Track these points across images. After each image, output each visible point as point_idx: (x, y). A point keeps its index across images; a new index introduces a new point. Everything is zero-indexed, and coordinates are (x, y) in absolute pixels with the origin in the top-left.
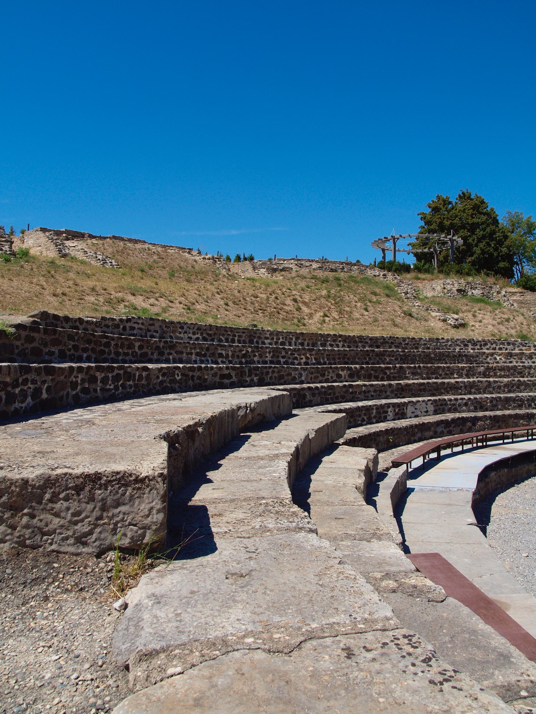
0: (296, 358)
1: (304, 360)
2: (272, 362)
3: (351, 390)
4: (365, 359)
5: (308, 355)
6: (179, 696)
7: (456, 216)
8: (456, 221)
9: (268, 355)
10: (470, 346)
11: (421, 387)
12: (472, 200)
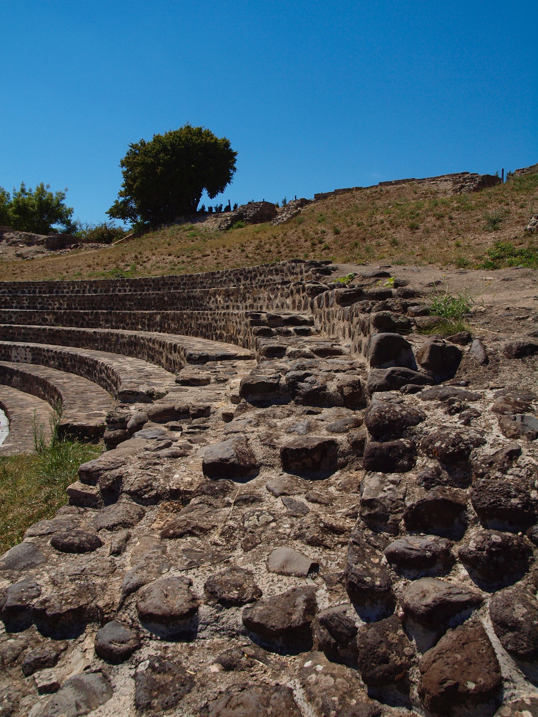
0: (50, 304)
1: (57, 306)
2: (28, 308)
3: (11, 331)
4: (110, 304)
5: (61, 301)
9: (25, 302)
11: (69, 335)
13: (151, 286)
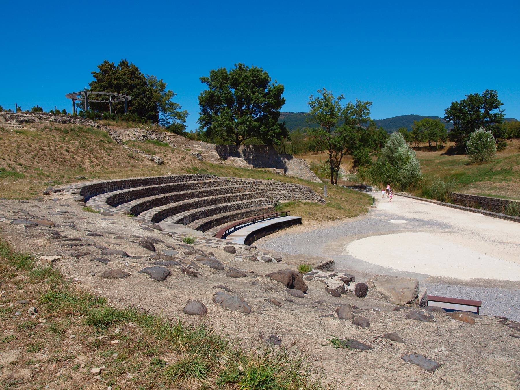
6: (428, 187)
7: (120, 78)
8: (120, 81)
10: (185, 180)
12: (129, 67)
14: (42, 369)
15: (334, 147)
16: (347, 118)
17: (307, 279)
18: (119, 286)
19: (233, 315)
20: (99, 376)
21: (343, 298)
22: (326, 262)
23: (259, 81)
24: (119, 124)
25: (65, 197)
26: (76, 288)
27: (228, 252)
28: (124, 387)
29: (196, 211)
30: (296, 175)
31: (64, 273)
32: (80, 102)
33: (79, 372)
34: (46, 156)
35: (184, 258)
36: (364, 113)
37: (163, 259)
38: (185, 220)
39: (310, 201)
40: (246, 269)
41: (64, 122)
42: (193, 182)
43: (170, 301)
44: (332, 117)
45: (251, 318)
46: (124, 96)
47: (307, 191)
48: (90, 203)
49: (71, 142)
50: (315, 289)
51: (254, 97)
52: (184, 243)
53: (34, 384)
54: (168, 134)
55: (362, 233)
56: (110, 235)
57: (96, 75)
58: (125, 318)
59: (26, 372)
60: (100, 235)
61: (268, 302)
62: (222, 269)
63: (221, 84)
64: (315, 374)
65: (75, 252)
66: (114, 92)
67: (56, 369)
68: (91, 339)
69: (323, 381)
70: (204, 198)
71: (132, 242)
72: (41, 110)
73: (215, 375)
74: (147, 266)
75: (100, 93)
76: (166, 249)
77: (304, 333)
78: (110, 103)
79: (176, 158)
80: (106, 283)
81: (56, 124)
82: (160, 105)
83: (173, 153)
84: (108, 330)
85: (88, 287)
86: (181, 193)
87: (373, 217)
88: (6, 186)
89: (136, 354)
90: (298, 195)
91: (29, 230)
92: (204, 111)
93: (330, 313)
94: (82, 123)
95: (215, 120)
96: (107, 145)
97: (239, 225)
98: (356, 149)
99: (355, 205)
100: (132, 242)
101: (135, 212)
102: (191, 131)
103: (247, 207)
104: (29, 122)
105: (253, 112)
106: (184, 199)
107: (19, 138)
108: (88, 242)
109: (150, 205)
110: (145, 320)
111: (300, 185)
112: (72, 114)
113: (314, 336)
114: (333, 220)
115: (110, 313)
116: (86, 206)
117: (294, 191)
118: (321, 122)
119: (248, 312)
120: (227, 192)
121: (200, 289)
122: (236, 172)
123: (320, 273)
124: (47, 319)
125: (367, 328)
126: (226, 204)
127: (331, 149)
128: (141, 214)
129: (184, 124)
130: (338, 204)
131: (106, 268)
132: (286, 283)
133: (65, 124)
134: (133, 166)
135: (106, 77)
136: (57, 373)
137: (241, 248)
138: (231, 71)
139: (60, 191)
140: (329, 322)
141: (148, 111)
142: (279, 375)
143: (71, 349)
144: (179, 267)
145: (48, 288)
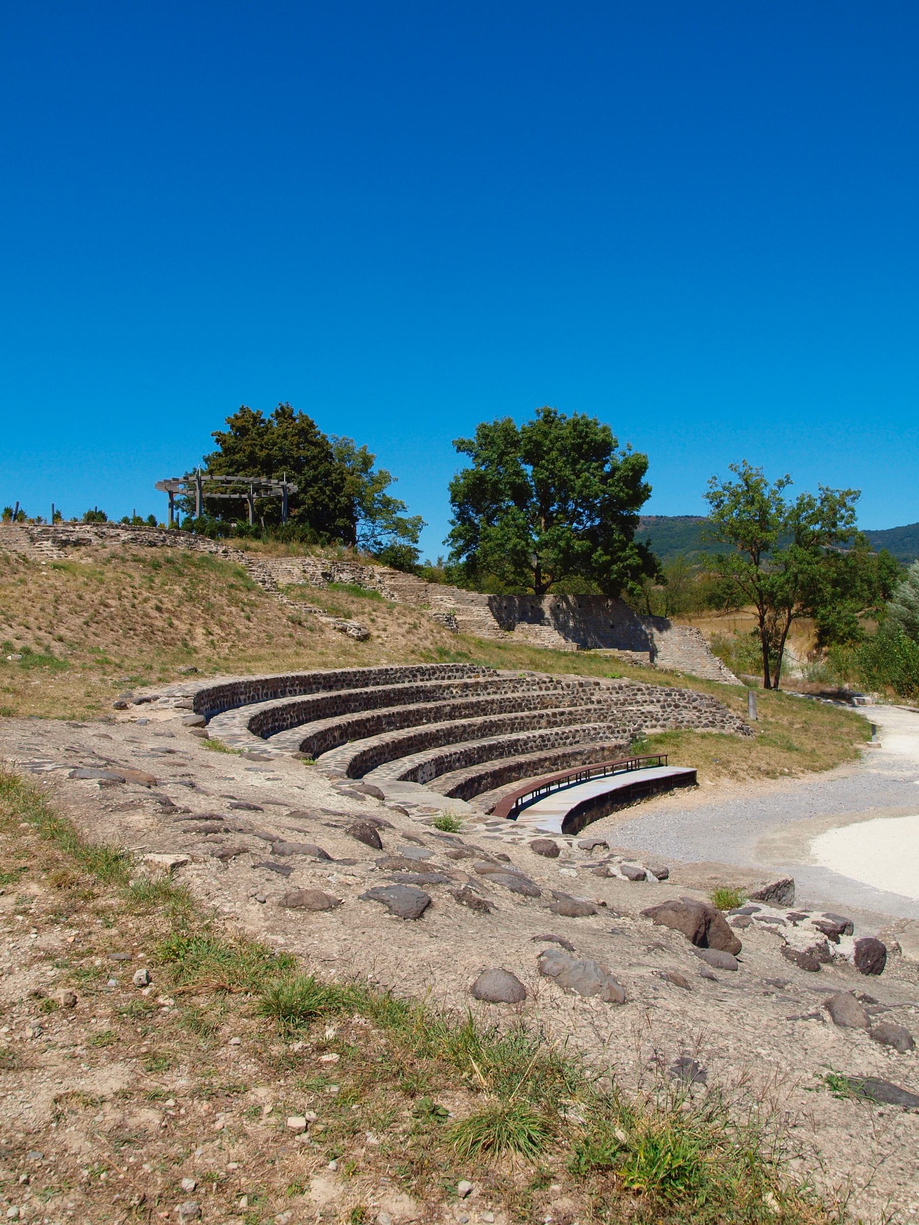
7: (275, 444)
8: (275, 452)
12: (295, 419)
13: (320, 683)
14: (183, 1111)
15: (767, 599)
16: (799, 530)
17: (737, 923)
18: (320, 929)
19: (586, 1006)
20: (305, 1136)
21: (827, 974)
22: (773, 883)
23: (591, 447)
24: (269, 547)
25: (162, 716)
26: (226, 929)
27: (540, 853)
28: (362, 1164)
29: (446, 750)
30: (678, 667)
31: (198, 894)
32: (183, 497)
33: (262, 1123)
34: (112, 619)
35: (448, 866)
36: (842, 517)
37: (410, 869)
38: (420, 773)
39: (715, 731)
40: (587, 895)
41: (152, 544)
42: (439, 682)
43: (439, 967)
44: (762, 529)
45: (628, 1014)
46: (281, 485)
47: (708, 706)
48: (214, 729)
49: (167, 588)
50: (758, 949)
51: (579, 482)
52: (438, 831)
53: (171, 1145)
54: (379, 569)
55: (849, 811)
56: (277, 807)
57: (220, 439)
58: (344, 1004)
59: (149, 1117)
60: (256, 809)
61: (662, 977)
62: (538, 894)
63: (502, 454)
64: (800, 1161)
65: (217, 847)
66: (259, 475)
67: (211, 1114)
68: (277, 1049)
69: (818, 1178)
70: (464, 721)
71: (327, 825)
72: (103, 517)
73: (562, 1148)
74: (377, 885)
75: (229, 478)
76: (403, 842)
77: (758, 1056)
78: (251, 499)
79: (399, 625)
80: (291, 921)
81: (135, 549)
82: (360, 504)
83: (391, 613)
84: (310, 1031)
85: (251, 927)
86: (412, 707)
87: (874, 771)
88: (36, 688)
89: (378, 1089)
90: (688, 715)
91: (109, 791)
92: (462, 517)
93: (812, 1010)
94: (191, 546)
95: (488, 536)
96: (243, 596)
97: (548, 785)
98: (824, 603)
99: (827, 741)
100: (327, 825)
101: (312, 749)
102: (428, 562)
103: (565, 744)
104: (78, 543)
105: (575, 517)
106: (418, 723)
107: (58, 580)
108: (239, 825)
109: (341, 736)
110: (390, 1012)
111: (691, 690)
112: (167, 525)
113: (783, 1064)
114: (775, 778)
115: (312, 988)
116: (207, 737)
117: (677, 706)
118: (737, 539)
119: (619, 1001)
120: (516, 706)
121: (503, 943)
122: (538, 658)
123: (766, 910)
124: (175, 998)
125: (908, 1052)
126: (514, 736)
127: (762, 603)
128: (321, 757)
129: (415, 546)
130: (784, 737)
131: (288, 887)
132: (691, 933)
133: (154, 549)
134: (300, 644)
135: (245, 444)
136: (214, 1122)
137: (570, 844)
138: (527, 425)
139: (148, 700)
140: (812, 1032)
141: (336, 517)
142: (711, 1157)
143: (235, 1069)
144: (448, 887)
145: (166, 927)
